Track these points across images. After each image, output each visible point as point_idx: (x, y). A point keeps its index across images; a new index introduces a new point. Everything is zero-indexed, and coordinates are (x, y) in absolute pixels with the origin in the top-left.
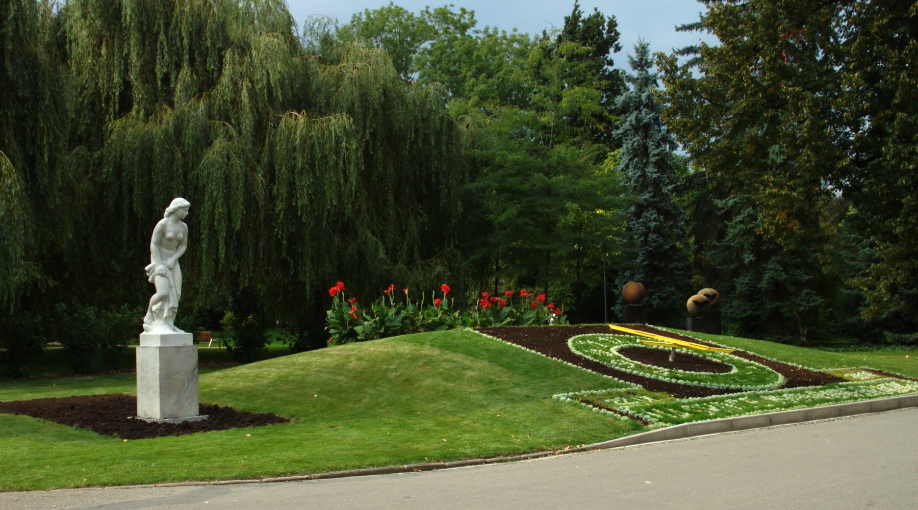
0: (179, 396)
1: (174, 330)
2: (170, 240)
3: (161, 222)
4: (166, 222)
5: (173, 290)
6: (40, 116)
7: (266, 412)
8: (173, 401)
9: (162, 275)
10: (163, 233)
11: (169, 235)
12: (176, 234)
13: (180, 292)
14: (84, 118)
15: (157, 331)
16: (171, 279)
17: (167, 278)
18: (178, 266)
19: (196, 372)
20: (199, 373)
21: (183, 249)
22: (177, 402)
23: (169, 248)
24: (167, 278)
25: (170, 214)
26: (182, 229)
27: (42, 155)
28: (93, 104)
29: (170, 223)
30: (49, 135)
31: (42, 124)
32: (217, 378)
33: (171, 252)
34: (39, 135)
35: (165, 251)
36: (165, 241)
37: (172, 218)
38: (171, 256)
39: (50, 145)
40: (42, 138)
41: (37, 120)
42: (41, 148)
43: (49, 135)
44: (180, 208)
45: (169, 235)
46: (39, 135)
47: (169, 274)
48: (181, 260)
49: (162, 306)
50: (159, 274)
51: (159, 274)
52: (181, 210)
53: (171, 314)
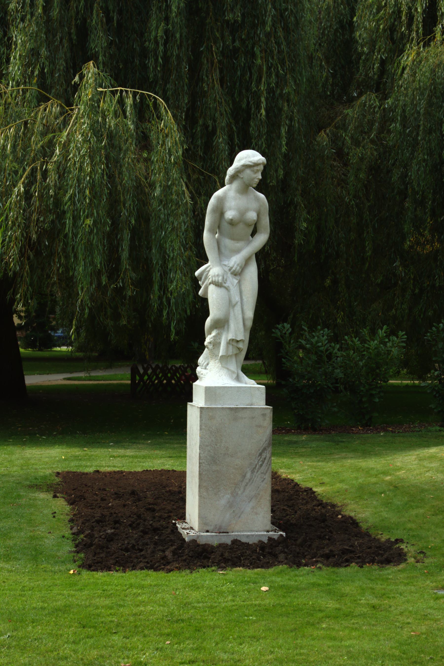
0: (234, 494)
1: (238, 379)
2: (232, 223)
3: (219, 193)
4: (225, 193)
5: (238, 309)
6: (257, 50)
7: (204, 543)
8: (223, 502)
9: (218, 285)
10: (220, 211)
11: (230, 214)
12: (243, 213)
13: (250, 314)
14: (379, 51)
15: (218, 377)
16: (234, 291)
17: (227, 289)
18: (252, 272)
19: (267, 454)
20: (273, 454)
21: (261, 239)
22: (231, 505)
23: (233, 238)
24: (227, 289)
25: (234, 177)
26: (254, 205)
27: (258, 108)
28: (392, 29)
29: (232, 194)
30: (269, 76)
31: (259, 61)
32: (91, 466)
33: (239, 245)
34: (255, 77)
35: (227, 242)
36: (225, 225)
37: (235, 185)
38: (238, 251)
39: (270, 91)
40: (259, 81)
41: (254, 55)
42: (257, 96)
43: (269, 76)
44: (246, 167)
45: (230, 214)
46: (255, 77)
47: (232, 282)
48: (261, 256)
49: (218, 336)
50: (213, 283)
51: (213, 283)
52: (248, 172)
53: (231, 351)
